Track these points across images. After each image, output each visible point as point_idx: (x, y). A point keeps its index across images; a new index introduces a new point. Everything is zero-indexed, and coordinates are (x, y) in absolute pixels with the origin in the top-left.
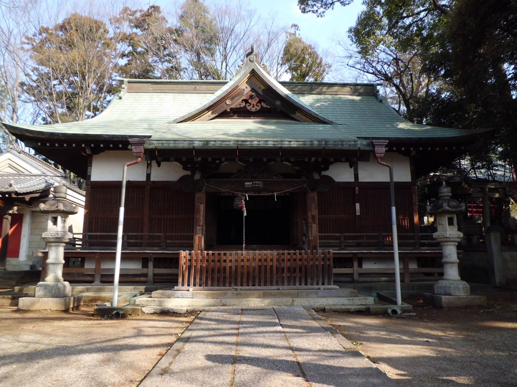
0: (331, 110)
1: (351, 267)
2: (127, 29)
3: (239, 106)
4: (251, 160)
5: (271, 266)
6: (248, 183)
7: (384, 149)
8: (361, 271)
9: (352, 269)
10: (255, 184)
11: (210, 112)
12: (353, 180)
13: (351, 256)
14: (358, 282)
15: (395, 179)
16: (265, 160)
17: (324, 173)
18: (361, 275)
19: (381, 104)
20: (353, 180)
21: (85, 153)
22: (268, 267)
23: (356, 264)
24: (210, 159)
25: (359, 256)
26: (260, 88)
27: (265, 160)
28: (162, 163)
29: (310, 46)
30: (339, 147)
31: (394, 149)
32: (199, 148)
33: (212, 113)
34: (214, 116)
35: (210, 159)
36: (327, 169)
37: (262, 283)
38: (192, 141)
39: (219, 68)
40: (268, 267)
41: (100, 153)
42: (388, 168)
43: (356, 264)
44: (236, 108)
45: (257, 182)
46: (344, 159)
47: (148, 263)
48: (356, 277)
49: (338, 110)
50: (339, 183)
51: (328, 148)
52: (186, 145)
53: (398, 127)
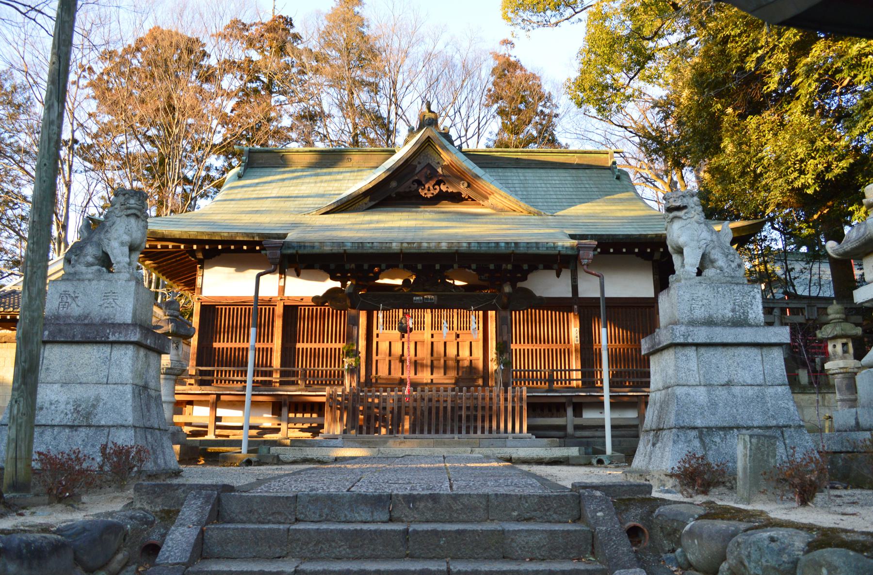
0: (543, 193)
1: (563, 417)
2: (239, 53)
3: (407, 190)
4: (420, 267)
5: (445, 408)
6: (418, 298)
7: (591, 254)
8: (578, 421)
9: (565, 419)
10: (427, 299)
11: (368, 199)
12: (570, 295)
13: (563, 400)
14: (573, 437)
15: (609, 294)
16: (438, 267)
17: (520, 285)
18: (577, 427)
19: (618, 182)
20: (570, 295)
21: (194, 256)
22: (441, 408)
23: (570, 411)
24: (366, 267)
25: (574, 400)
26: (419, 163)
27: (438, 267)
28: (302, 271)
29: (534, 77)
30: (534, 251)
31: (637, 250)
32: (351, 251)
33: (370, 201)
34: (374, 203)
35: (366, 267)
36: (525, 279)
37: (433, 431)
38: (343, 244)
39: (385, 115)
40: (441, 408)
41: (214, 256)
42: (261, 278)
43: (570, 411)
44: (405, 192)
45: (429, 297)
46: (541, 266)
47: (281, 410)
48: (570, 430)
49: (552, 193)
50: (541, 298)
51: (518, 252)
52: (336, 250)
53: (331, 284)
